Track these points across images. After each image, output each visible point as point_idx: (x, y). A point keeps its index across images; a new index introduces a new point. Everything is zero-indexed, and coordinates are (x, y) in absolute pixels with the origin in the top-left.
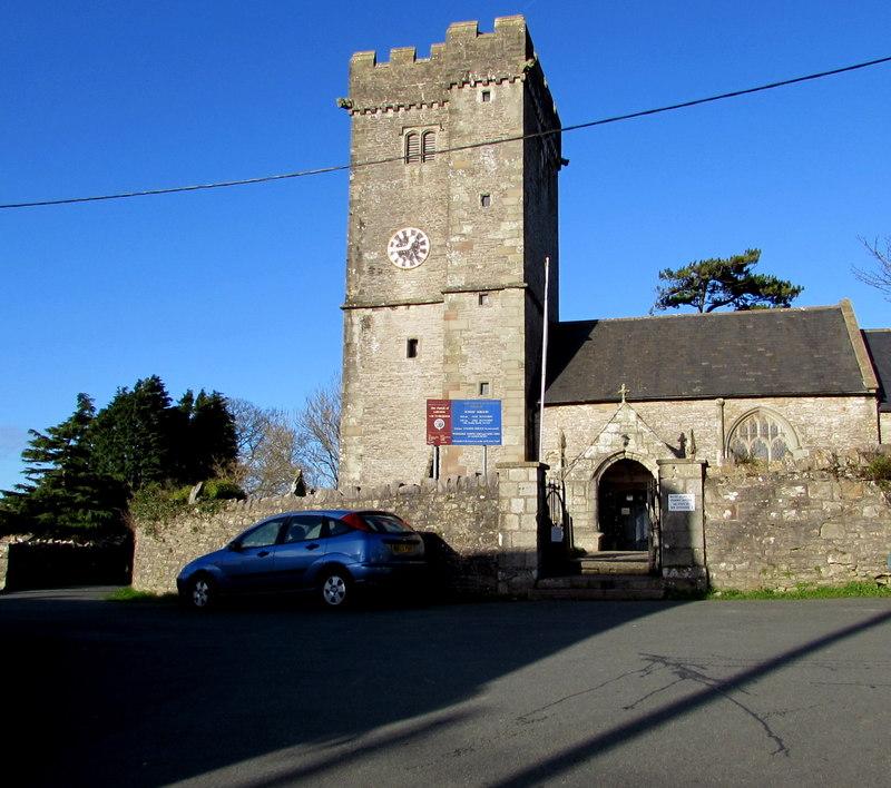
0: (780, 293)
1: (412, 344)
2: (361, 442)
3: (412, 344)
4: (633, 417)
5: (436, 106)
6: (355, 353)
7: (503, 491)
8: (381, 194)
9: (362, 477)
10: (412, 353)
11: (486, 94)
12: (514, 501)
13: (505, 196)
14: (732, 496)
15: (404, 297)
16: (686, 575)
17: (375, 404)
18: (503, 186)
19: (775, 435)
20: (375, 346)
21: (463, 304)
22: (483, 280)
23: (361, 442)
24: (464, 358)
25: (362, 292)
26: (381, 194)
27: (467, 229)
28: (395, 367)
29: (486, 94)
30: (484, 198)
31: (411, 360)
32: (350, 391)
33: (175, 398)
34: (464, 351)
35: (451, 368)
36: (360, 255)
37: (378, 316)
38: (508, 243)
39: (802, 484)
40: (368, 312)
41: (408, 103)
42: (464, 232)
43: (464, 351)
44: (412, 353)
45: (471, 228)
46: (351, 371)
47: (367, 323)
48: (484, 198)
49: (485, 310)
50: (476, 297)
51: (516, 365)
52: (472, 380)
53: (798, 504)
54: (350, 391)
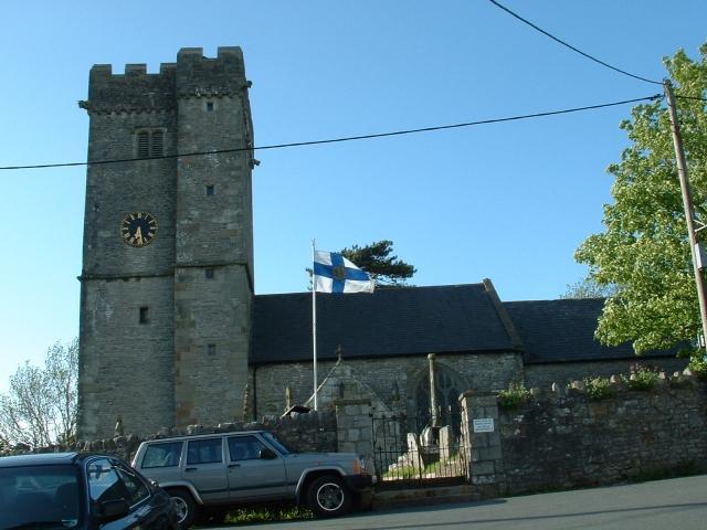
0: (405, 270)
2: (97, 398)
3: (143, 310)
4: (348, 372)
5: (163, 112)
6: (91, 319)
7: (340, 424)
8: (114, 181)
10: (143, 320)
11: (210, 105)
12: (351, 432)
13: (226, 187)
14: (520, 419)
15: (135, 270)
16: (491, 481)
18: (226, 179)
19: (449, 385)
21: (192, 278)
22: (210, 257)
23: (97, 398)
26: (114, 181)
28: (127, 332)
29: (210, 105)
30: (210, 189)
34: (193, 317)
38: (230, 227)
39: (567, 407)
40: (102, 283)
43: (193, 317)
48: (210, 189)
50: (203, 272)
51: (239, 330)
52: (201, 342)
53: (568, 420)
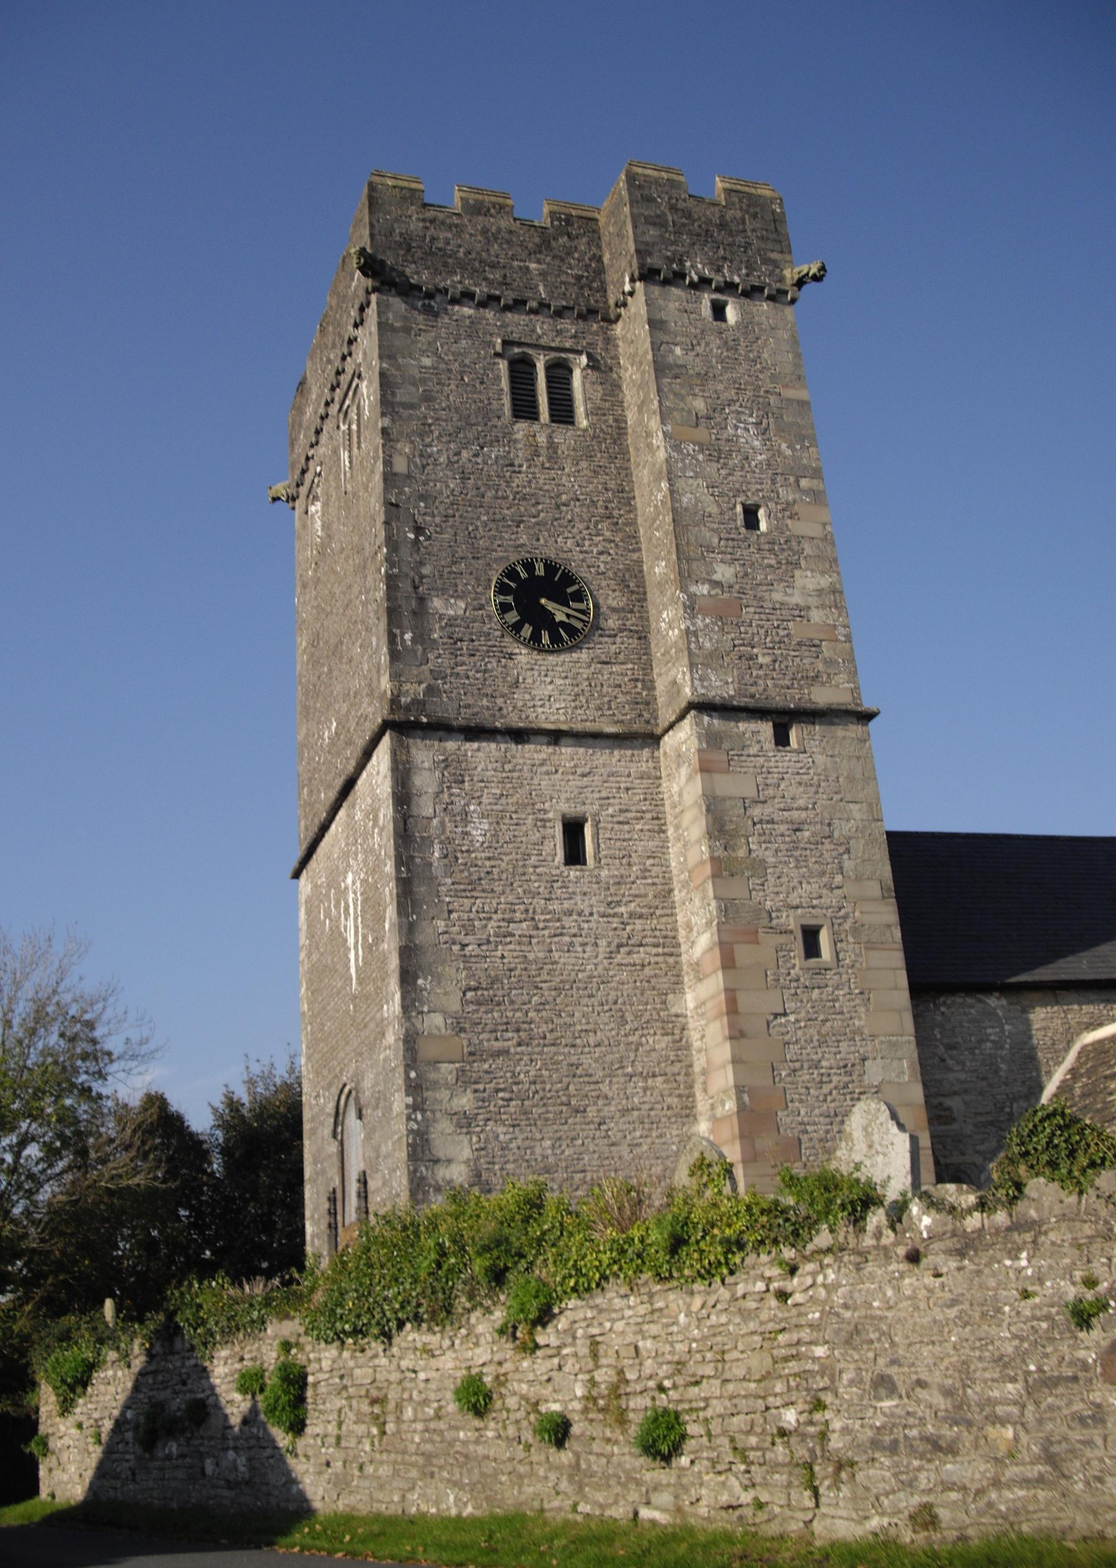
1: (573, 830)
3: (573, 830)
6: (428, 842)
9: (477, 1176)
10: (574, 855)
15: (550, 716)
17: (495, 980)
20: (479, 830)
24: (759, 867)
25: (431, 690)
27: (724, 572)
31: (573, 872)
32: (420, 939)
33: (200, 1120)
35: (737, 889)
36: (422, 600)
37: (483, 755)
41: (508, 297)
42: (716, 577)
44: (574, 855)
45: (732, 570)
46: (421, 890)
47: (455, 774)
49: (784, 761)
50: (766, 729)
51: (873, 889)
54: (420, 939)
